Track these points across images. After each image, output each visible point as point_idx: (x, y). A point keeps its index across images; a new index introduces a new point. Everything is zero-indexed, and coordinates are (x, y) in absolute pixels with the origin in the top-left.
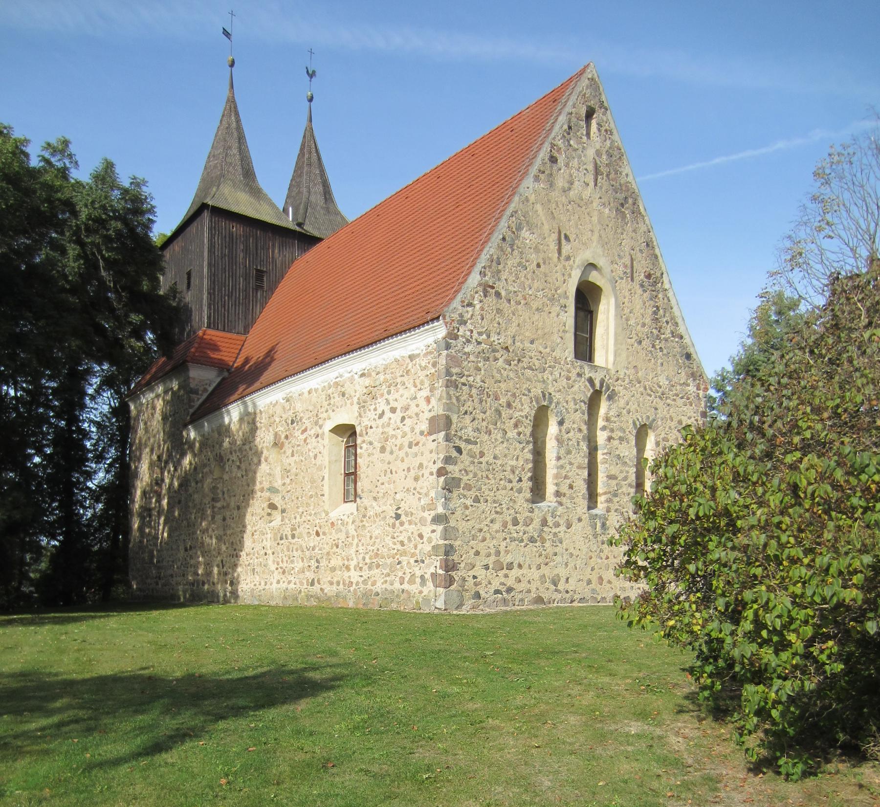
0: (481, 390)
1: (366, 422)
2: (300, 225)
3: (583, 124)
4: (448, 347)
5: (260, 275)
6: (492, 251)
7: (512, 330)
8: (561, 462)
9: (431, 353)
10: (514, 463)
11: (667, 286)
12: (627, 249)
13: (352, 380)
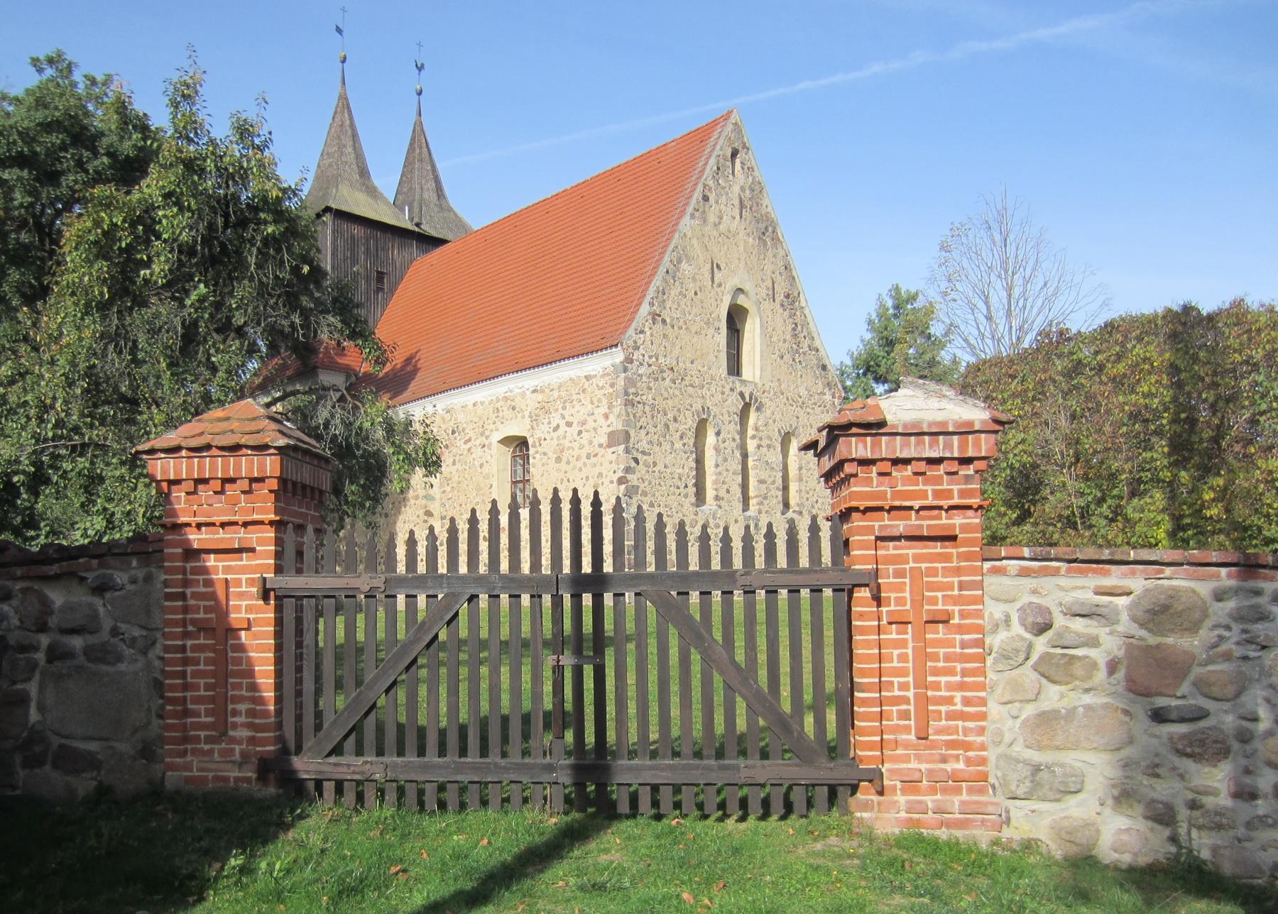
0: (653, 407)
1: (538, 434)
2: (418, 225)
3: (729, 164)
4: (625, 370)
5: (380, 276)
6: (658, 283)
7: (676, 352)
8: (720, 469)
9: (608, 374)
10: (680, 471)
11: (803, 304)
12: (769, 273)
13: (523, 395)
